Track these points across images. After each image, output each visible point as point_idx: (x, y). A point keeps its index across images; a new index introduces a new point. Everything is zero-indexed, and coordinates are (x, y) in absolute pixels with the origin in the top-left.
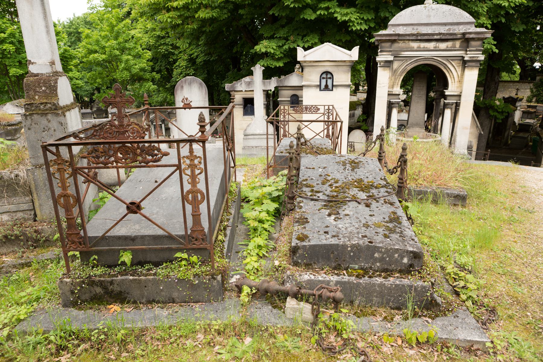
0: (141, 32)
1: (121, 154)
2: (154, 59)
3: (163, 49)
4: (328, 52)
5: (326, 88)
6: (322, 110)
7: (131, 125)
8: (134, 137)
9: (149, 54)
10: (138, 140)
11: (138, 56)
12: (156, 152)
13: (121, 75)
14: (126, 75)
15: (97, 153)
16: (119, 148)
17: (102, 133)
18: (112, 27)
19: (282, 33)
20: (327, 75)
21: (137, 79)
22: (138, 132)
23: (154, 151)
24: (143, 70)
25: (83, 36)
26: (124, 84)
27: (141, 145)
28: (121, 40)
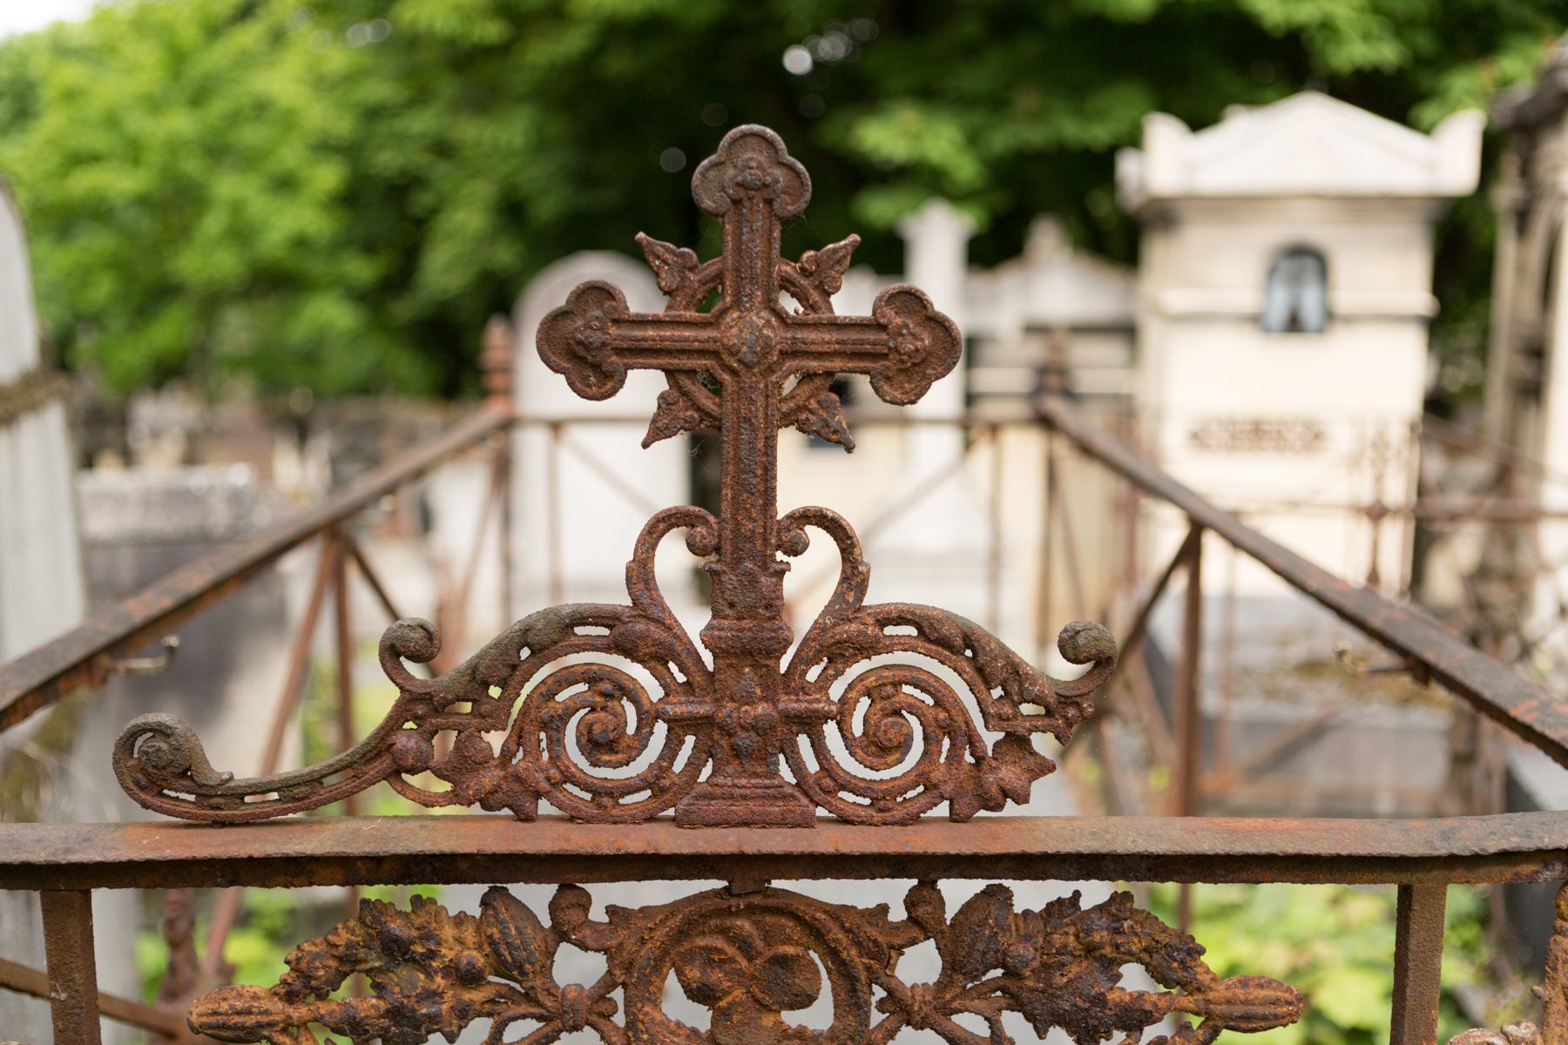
0: (302, 75)
1: (700, 994)
2: (349, 199)
3: (387, 160)
4: (1299, 145)
5: (1294, 324)
6: (1342, 439)
7: (867, 648)
8: (881, 797)
9: (328, 177)
10: (935, 835)
11: (285, 185)
12: (1134, 979)
13: (205, 259)
14: (225, 264)
15: (406, 982)
16: (692, 916)
17: (496, 740)
18: (178, 58)
19: (976, 78)
20: (1305, 260)
21: (275, 282)
22: (947, 724)
23: (1111, 968)
24: (301, 243)
25: (48, 94)
26: (212, 302)
27: (956, 892)
28: (218, 107)
